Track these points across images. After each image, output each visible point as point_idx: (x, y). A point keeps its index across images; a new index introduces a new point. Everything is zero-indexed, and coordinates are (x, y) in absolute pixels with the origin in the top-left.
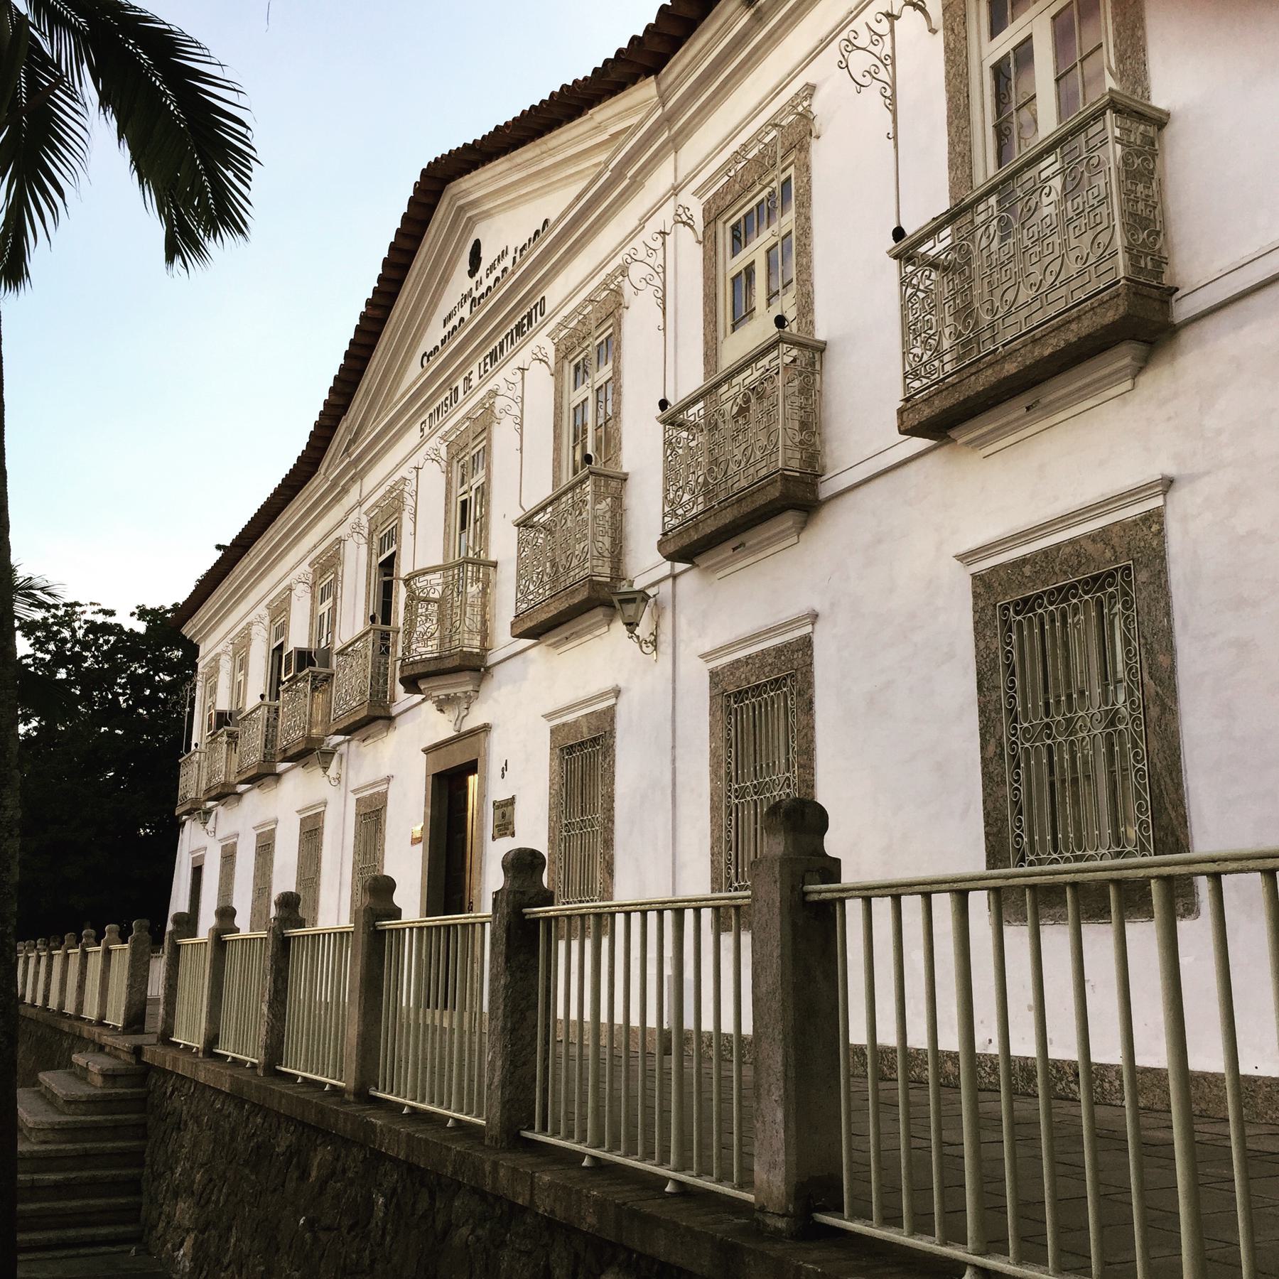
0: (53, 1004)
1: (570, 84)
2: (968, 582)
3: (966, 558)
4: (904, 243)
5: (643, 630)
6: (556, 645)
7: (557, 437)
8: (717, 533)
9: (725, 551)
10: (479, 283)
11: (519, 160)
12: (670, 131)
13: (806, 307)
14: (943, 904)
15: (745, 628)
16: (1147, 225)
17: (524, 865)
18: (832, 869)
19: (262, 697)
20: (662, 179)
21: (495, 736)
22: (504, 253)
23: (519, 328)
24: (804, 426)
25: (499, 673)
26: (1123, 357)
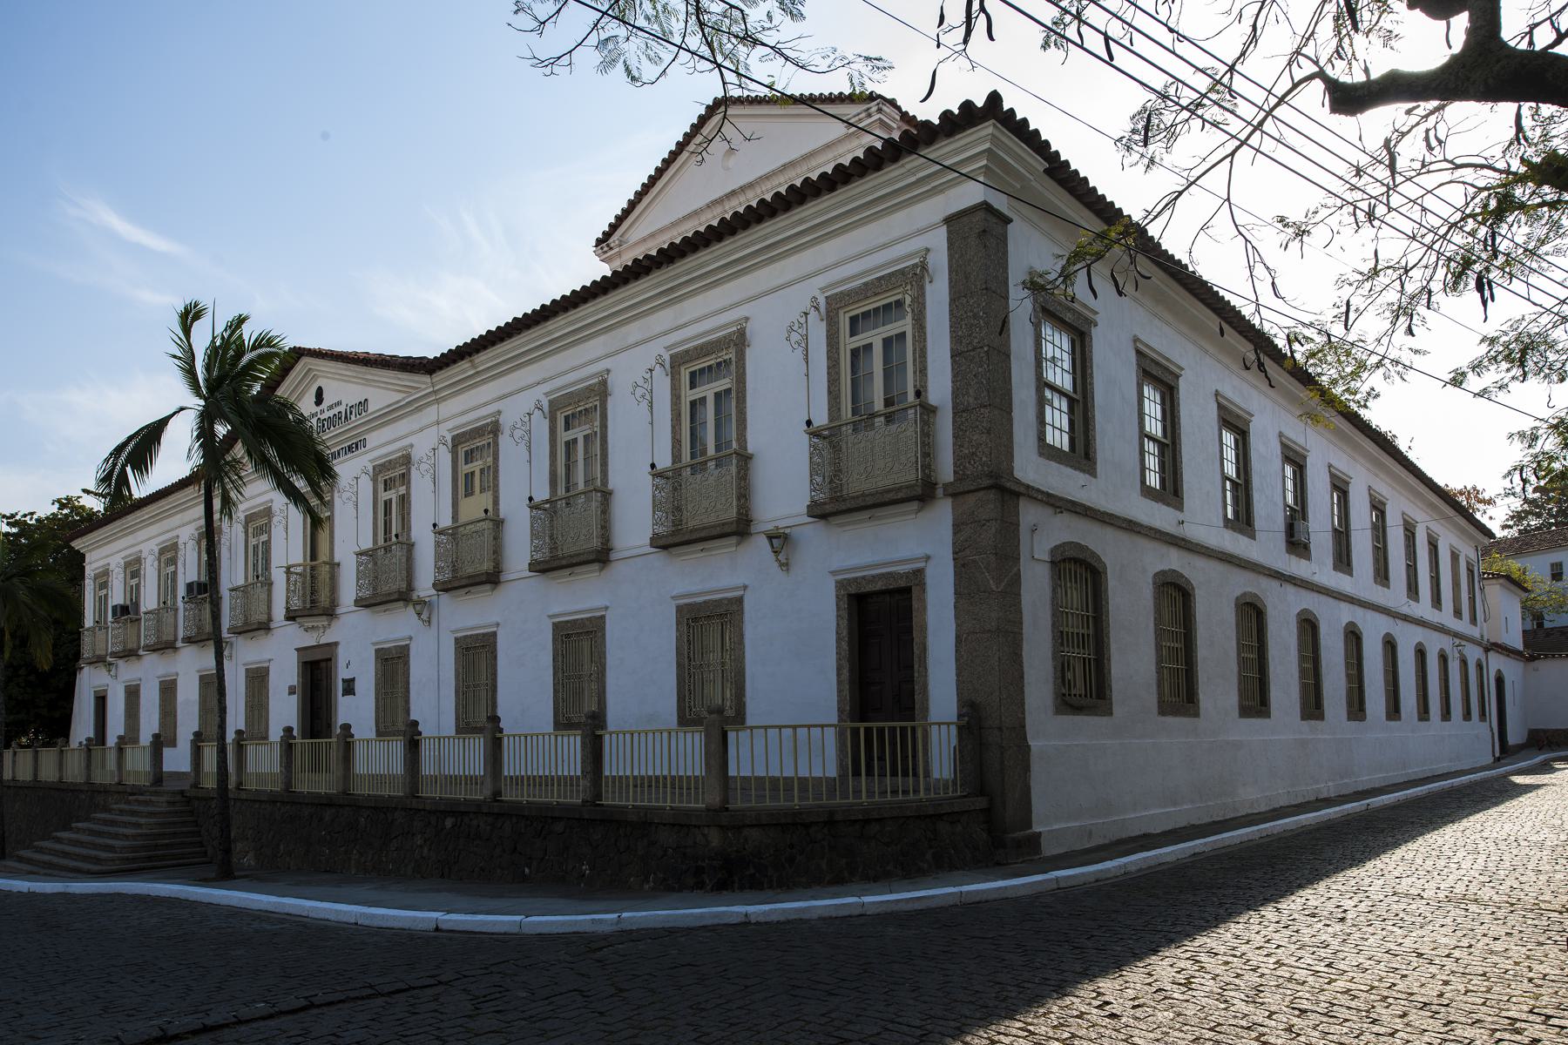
0: (689, 736)
1: (1019, 117)
2: (674, 610)
3: (833, 573)
4: (892, 409)
5: (425, 616)
6: (840, 525)
7: (375, 513)
8: (456, 583)
9: (865, 515)
10: (322, 412)
11: (908, 167)
12: (437, 398)
13: (496, 502)
14: (628, 736)
15: (694, 589)
16: (744, 495)
17: (239, 732)
18: (501, 731)
19: (486, 511)
20: (430, 414)
21: (341, 651)
22: (339, 403)
23: (350, 447)
24: (603, 527)
25: (343, 619)
26: (733, 540)
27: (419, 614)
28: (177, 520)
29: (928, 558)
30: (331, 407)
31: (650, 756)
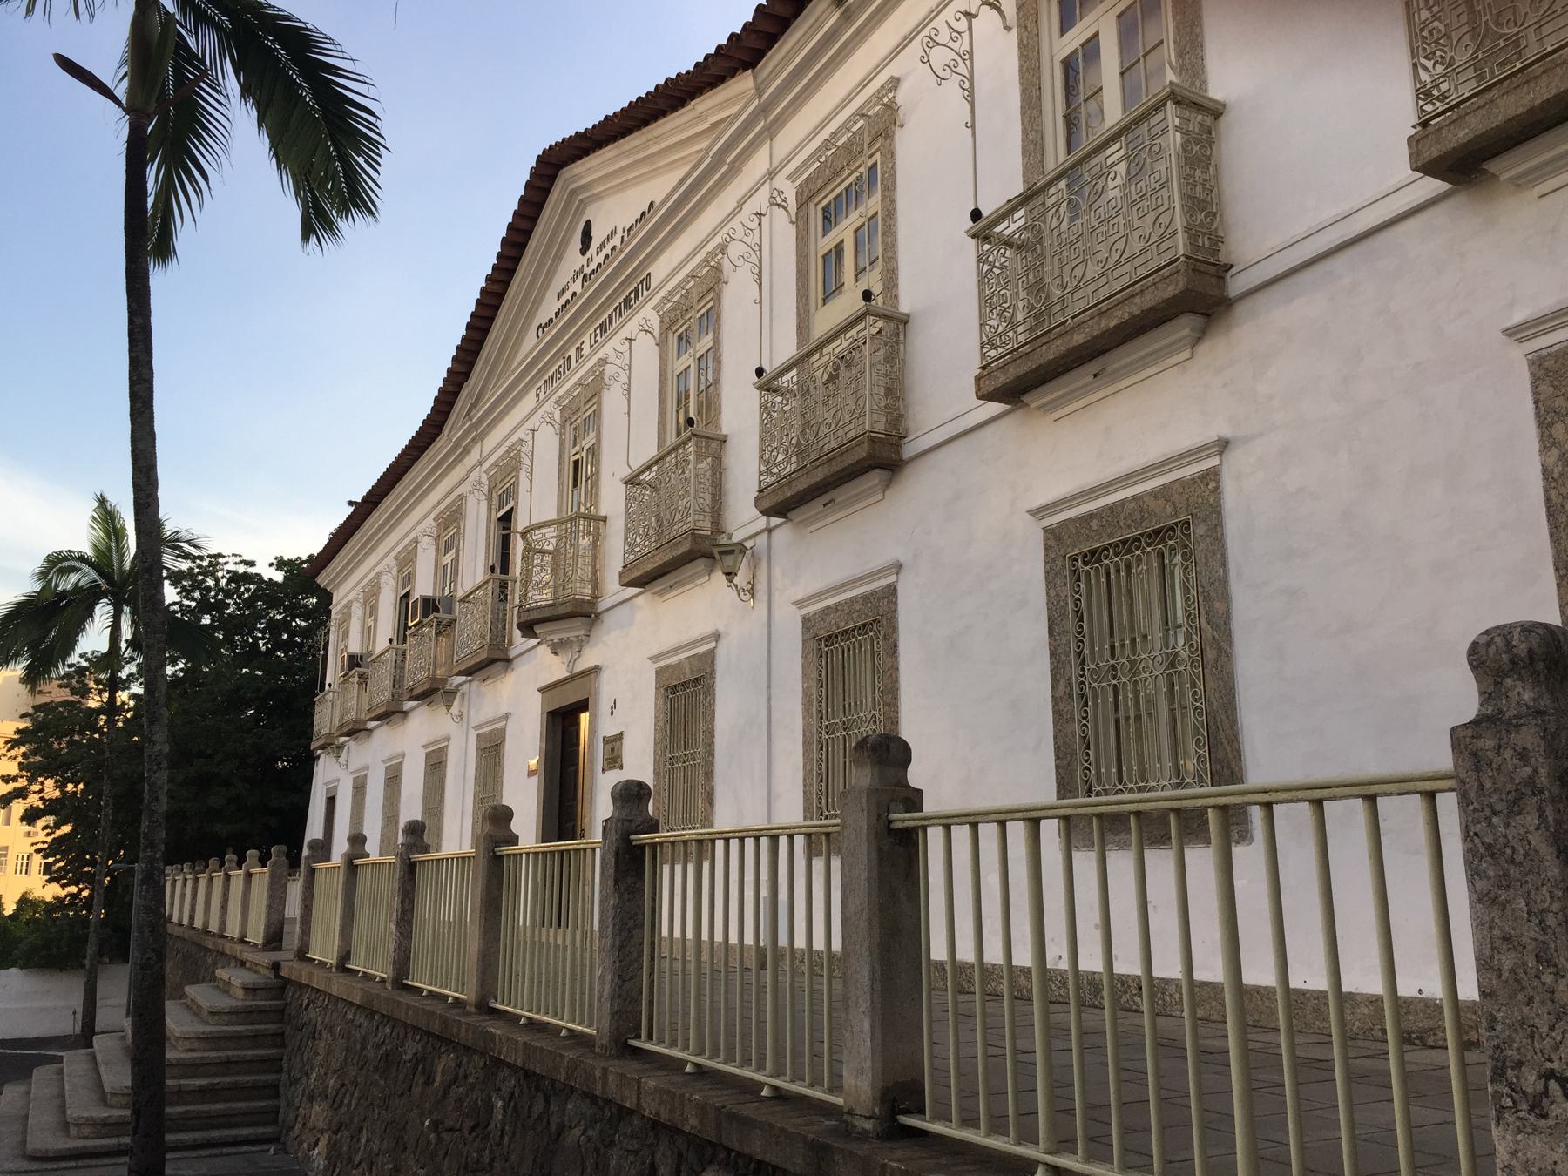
4: (981, 224)
5: (741, 579)
7: (662, 402)
9: (1083, 375)
10: (590, 260)
11: (626, 147)
12: (767, 120)
13: (891, 282)
14: (1017, 831)
16: (1205, 208)
17: (631, 795)
18: (913, 800)
20: (759, 164)
21: (605, 677)
22: (613, 233)
23: (627, 301)
24: (889, 391)
26: (1184, 327)
27: (730, 575)
28: (372, 560)
29: (898, 568)
30: (602, 246)
31: (991, 880)
